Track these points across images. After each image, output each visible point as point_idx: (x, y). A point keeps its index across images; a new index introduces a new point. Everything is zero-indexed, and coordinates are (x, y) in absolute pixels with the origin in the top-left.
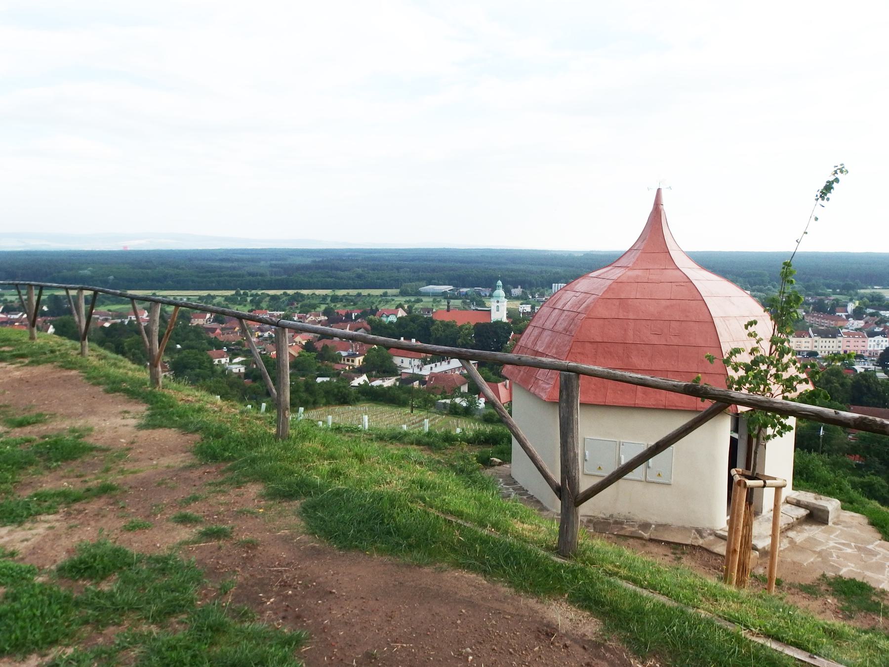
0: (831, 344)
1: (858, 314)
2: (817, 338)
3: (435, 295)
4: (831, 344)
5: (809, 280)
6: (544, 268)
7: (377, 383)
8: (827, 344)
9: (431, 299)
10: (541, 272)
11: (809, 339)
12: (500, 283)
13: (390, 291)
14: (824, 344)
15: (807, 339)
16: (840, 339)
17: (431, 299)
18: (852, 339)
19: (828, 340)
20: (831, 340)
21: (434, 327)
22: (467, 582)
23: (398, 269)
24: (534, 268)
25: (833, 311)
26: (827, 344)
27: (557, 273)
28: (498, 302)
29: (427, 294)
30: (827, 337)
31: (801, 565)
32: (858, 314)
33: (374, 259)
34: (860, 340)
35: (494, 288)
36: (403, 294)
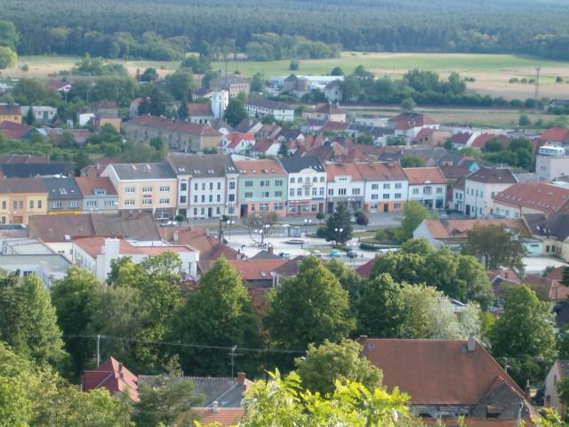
19: (207, 181)
20: (215, 181)
30: (205, 175)
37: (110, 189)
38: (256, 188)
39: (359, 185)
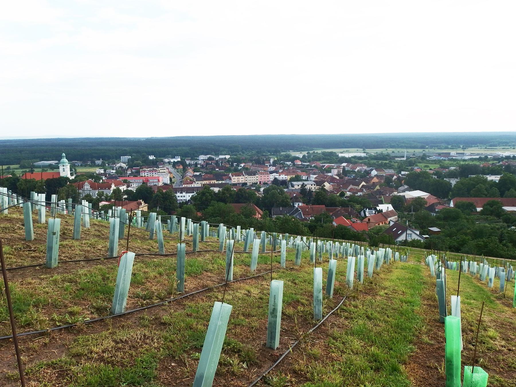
0: (253, 179)
1: (274, 164)
2: (246, 176)
3: (44, 167)
4: (253, 179)
5: (260, 149)
6: (119, 147)
7: (399, 194)
8: (252, 179)
9: (41, 170)
10: (116, 150)
11: (243, 177)
12: (64, 154)
13: (12, 166)
14: (250, 179)
15: (242, 177)
16: (257, 176)
17: (41, 170)
18: (263, 176)
20: (253, 176)
21: (18, 184)
22: (127, 272)
23: (21, 152)
24: (111, 148)
25: (264, 163)
26: (252, 179)
27: (125, 150)
28: (63, 166)
29: (39, 167)
31: (441, 174)
32: (274, 164)
33: (5, 146)
34: (266, 176)
35: (61, 157)
36: (22, 167)
37: (230, 179)
38: (263, 178)
39: (286, 176)
